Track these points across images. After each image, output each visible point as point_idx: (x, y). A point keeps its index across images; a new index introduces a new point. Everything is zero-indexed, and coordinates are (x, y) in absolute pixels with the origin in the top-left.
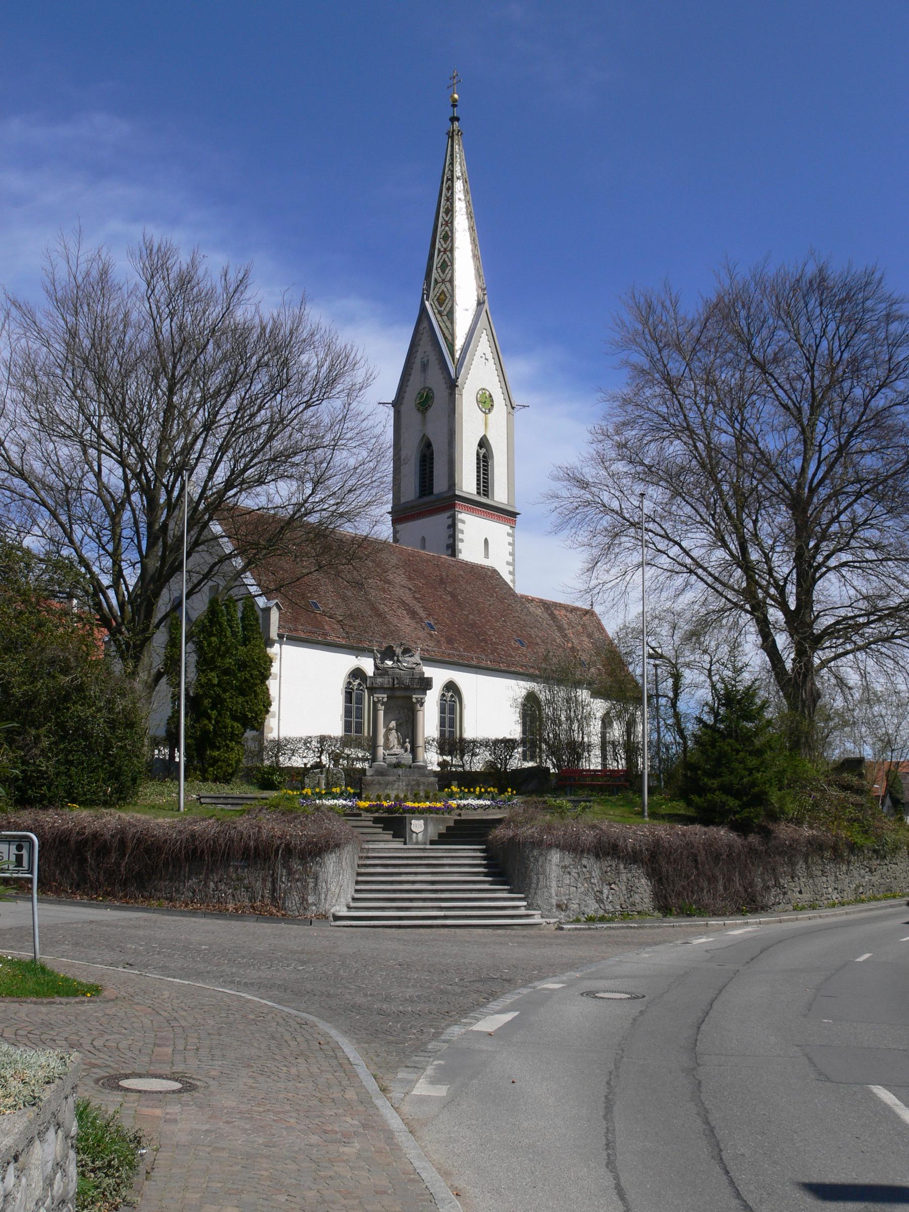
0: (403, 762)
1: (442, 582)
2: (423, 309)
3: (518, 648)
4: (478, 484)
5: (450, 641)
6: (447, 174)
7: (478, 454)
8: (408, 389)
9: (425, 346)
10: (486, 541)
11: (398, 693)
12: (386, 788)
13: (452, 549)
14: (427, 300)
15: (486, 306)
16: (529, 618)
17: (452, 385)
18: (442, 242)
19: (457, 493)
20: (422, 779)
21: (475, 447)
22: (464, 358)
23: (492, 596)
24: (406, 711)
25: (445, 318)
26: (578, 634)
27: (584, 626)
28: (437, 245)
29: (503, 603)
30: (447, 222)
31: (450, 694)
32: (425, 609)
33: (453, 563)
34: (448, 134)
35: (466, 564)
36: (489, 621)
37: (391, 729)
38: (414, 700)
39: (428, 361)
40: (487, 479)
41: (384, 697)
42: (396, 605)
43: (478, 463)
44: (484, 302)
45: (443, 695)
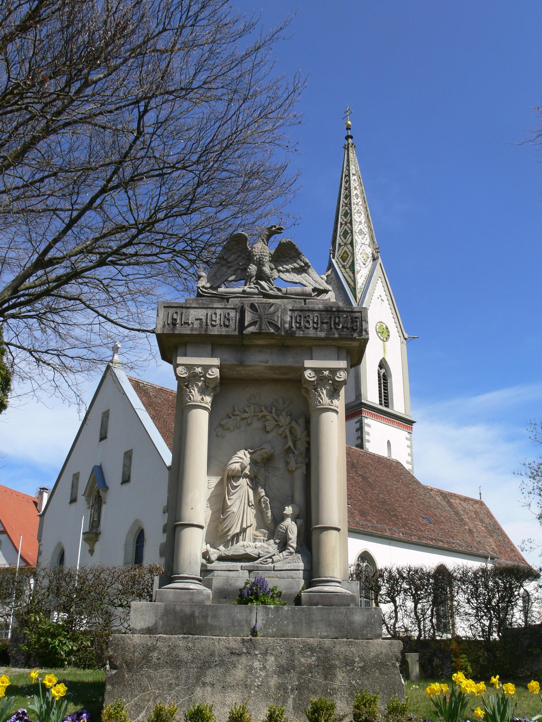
0: (272, 582)
3: (426, 524)
4: (380, 397)
5: (363, 514)
6: (345, 172)
7: (379, 374)
10: (389, 443)
11: (260, 361)
12: (199, 681)
13: (361, 446)
14: (334, 258)
15: (380, 261)
16: (432, 500)
18: (343, 218)
19: (363, 401)
20: (342, 648)
21: (377, 367)
22: (364, 297)
23: (398, 482)
24: (284, 420)
25: (348, 270)
26: (471, 518)
27: (476, 513)
28: (340, 220)
29: (408, 487)
30: (346, 204)
31: (365, 564)
33: (363, 454)
35: (370, 454)
36: (397, 500)
37: (234, 476)
38: (309, 375)
40: (387, 393)
41: (211, 364)
43: (379, 381)
44: (378, 258)
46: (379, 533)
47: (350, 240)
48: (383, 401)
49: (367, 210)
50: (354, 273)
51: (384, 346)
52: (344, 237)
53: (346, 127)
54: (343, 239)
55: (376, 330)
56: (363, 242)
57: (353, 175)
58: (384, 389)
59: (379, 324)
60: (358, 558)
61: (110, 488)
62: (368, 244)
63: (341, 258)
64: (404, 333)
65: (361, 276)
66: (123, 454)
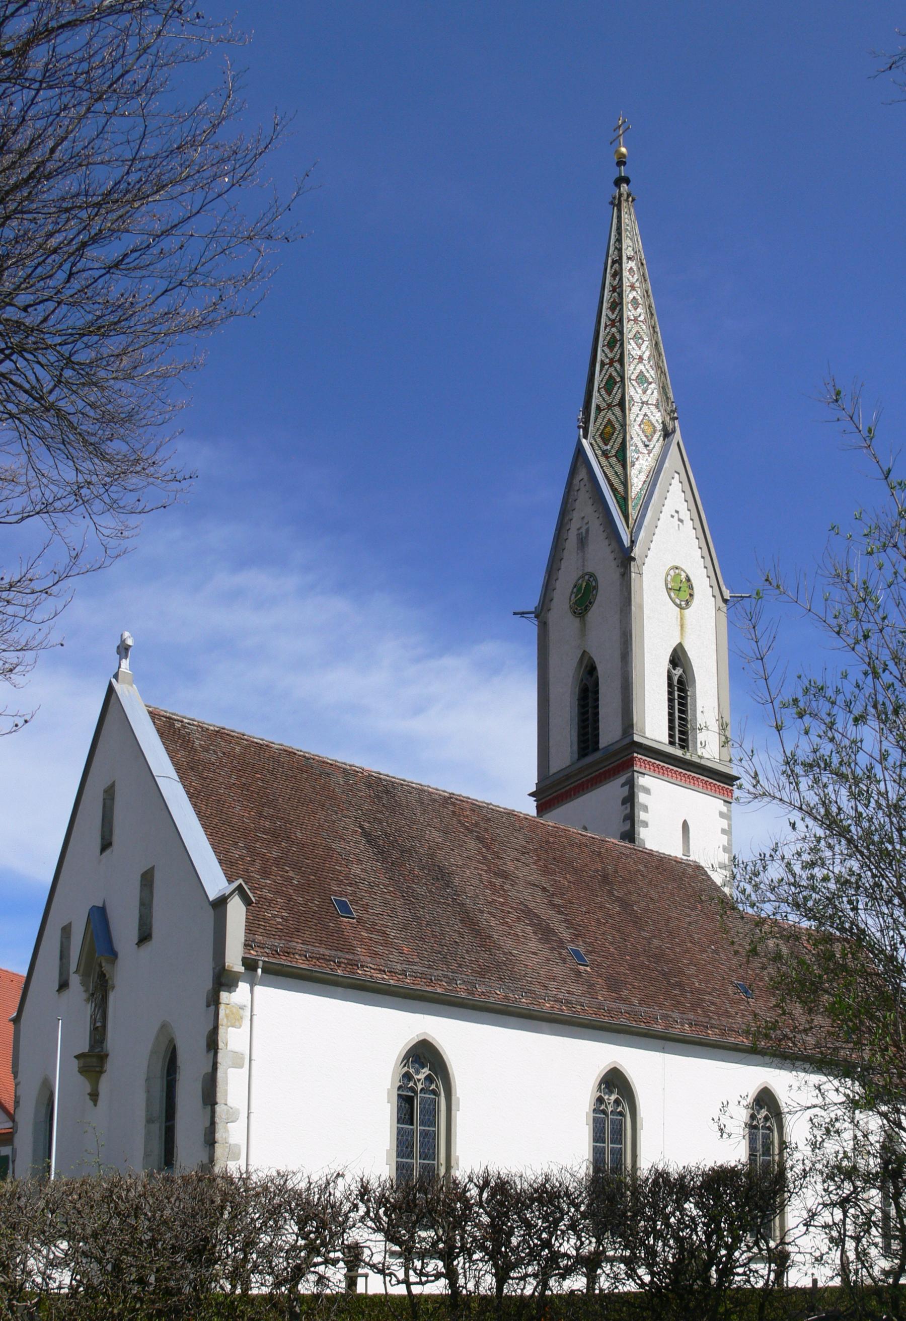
1: (605, 879)
2: (580, 450)
4: (671, 728)
5: (614, 985)
7: (670, 678)
8: (558, 585)
9: (584, 508)
10: (685, 825)
13: (630, 835)
14: (585, 437)
15: (678, 436)
17: (625, 559)
18: (607, 350)
19: (636, 738)
21: (665, 664)
22: (644, 516)
25: (613, 460)
30: (613, 321)
31: (613, 1097)
32: (569, 924)
34: (612, 203)
35: (651, 854)
36: (687, 951)
39: (587, 531)
42: (514, 915)
43: (670, 693)
44: (674, 431)
45: (600, 1100)
46: (643, 1025)
47: (619, 396)
48: (677, 735)
49: (655, 332)
50: (624, 466)
51: (681, 618)
52: (606, 391)
53: (616, 160)
54: (605, 396)
55: (666, 585)
56: (645, 399)
57: (629, 258)
58: (680, 711)
59: (672, 572)
60: (600, 1085)
61: (120, 956)
62: (654, 402)
63: (600, 435)
64: (724, 588)
65: (640, 472)
66: (139, 878)
